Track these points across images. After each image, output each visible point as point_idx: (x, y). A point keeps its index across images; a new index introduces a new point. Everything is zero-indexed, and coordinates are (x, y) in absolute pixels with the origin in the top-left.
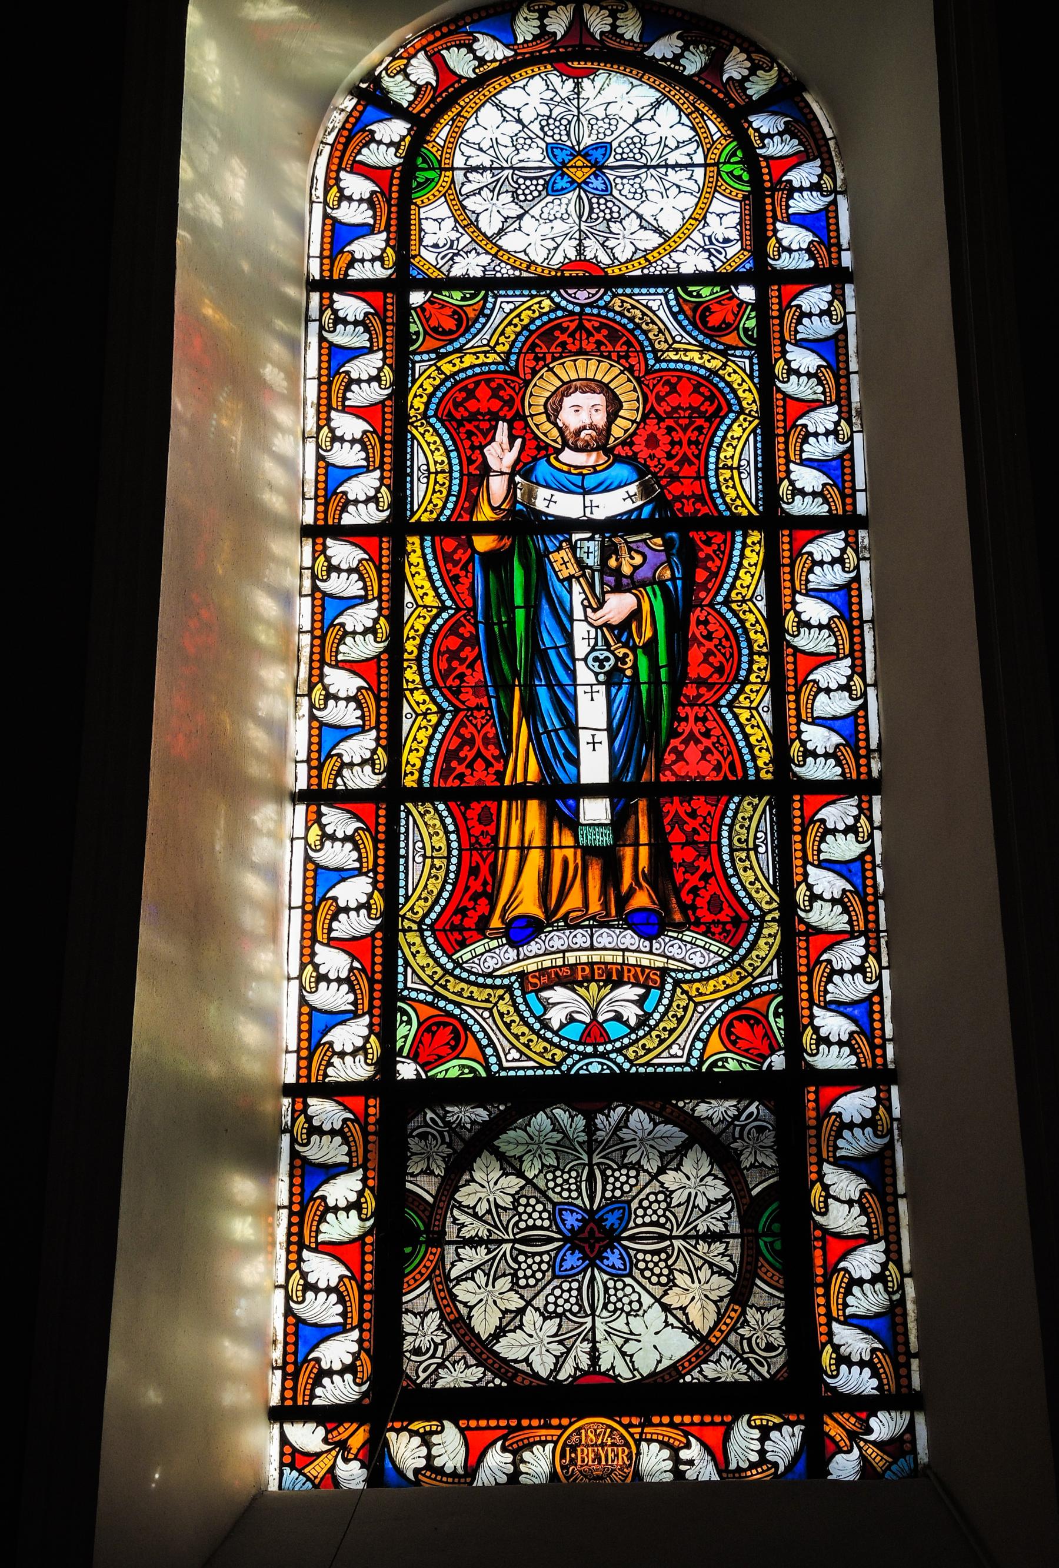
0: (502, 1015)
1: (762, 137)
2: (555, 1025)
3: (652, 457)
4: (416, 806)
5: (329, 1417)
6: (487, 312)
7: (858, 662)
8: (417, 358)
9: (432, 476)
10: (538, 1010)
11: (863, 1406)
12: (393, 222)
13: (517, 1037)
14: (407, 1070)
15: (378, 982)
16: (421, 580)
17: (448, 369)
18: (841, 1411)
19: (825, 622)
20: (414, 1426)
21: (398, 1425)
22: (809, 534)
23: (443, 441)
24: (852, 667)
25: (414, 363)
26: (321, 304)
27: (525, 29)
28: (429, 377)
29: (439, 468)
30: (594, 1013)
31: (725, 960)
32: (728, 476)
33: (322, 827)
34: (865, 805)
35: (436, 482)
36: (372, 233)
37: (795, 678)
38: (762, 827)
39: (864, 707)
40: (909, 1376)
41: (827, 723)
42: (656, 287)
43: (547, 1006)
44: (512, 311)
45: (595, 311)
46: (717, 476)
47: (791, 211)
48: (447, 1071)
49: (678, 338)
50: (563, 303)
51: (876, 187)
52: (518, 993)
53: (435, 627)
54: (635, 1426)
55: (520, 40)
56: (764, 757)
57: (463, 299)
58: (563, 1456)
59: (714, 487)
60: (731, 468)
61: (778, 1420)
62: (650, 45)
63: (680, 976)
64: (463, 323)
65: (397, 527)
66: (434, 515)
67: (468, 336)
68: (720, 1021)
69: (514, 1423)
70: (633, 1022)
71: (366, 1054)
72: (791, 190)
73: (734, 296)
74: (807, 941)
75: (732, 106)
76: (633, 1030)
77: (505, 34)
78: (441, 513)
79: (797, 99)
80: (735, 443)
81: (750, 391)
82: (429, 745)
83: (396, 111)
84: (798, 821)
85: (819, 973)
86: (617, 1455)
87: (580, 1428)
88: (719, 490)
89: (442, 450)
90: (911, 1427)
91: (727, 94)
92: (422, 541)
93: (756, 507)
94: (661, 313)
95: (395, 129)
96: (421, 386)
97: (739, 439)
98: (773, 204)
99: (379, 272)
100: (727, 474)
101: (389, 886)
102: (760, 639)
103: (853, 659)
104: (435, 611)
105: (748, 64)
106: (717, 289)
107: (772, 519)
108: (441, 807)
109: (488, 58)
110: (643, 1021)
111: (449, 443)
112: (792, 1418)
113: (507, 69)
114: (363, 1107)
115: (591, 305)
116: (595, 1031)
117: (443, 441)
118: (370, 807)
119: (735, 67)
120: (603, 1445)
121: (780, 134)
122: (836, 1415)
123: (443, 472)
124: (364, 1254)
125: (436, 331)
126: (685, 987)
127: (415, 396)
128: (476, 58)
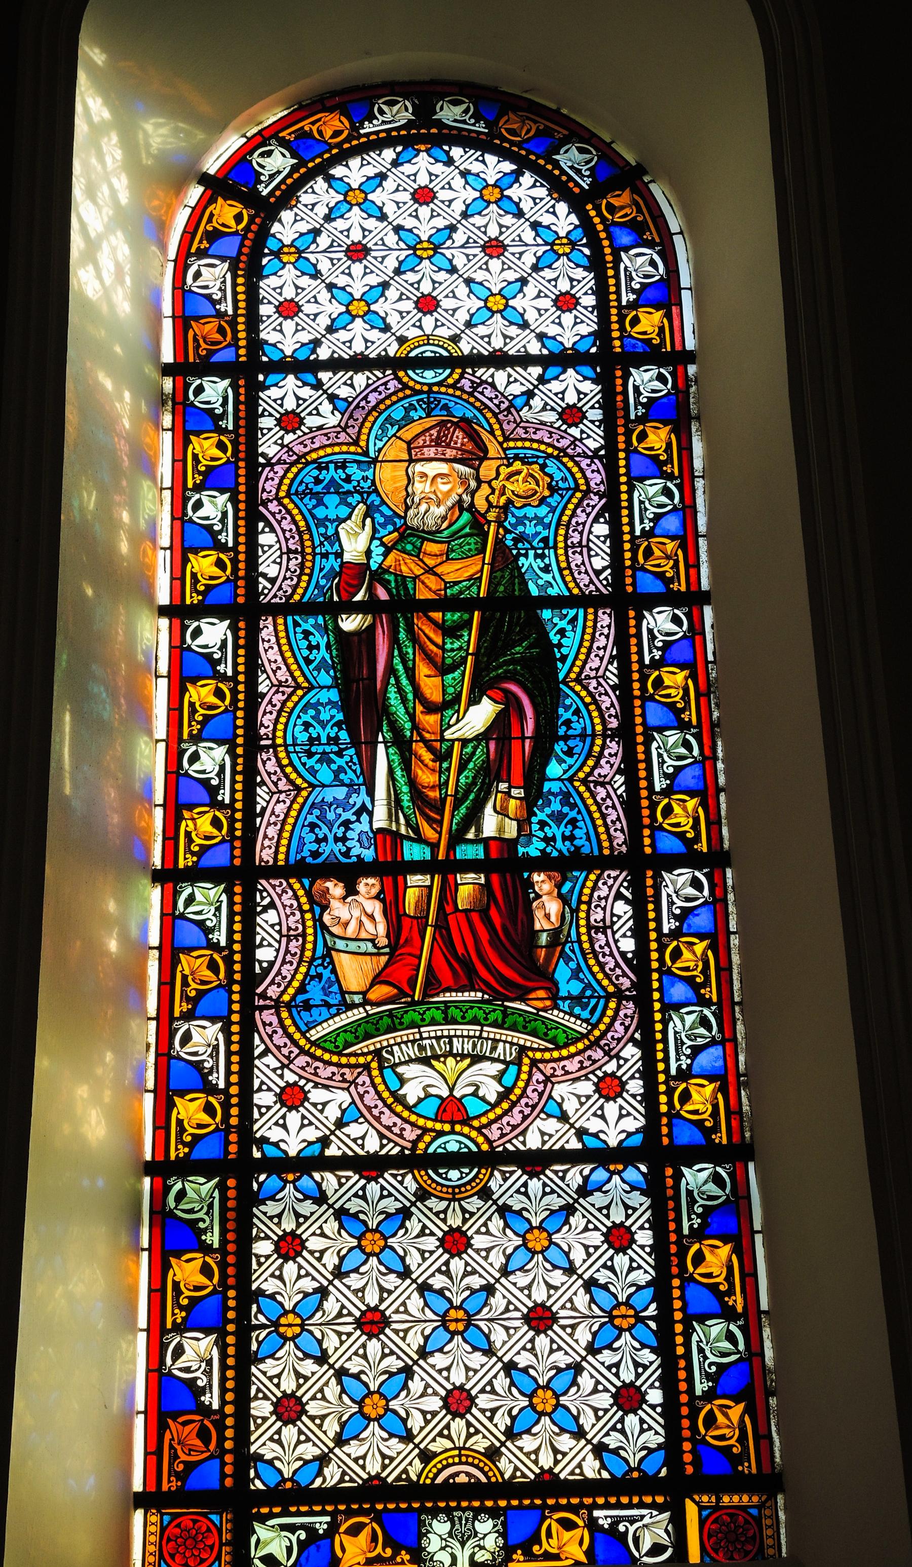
2: (411, 1100)
10: (394, 1084)
15: (230, 1368)
16: (273, 654)
30: (451, 1090)
43: (402, 1081)
45: (443, 389)
50: (474, 1134)
51: (721, 267)
52: (375, 1073)
56: (620, 838)
63: (538, 1055)
70: (492, 1098)
76: (493, 1106)
81: (264, 1024)
110: (503, 1096)
114: (217, 1475)
115: (441, 1134)
116: (451, 1108)
124: (231, 1002)
126: (541, 1066)
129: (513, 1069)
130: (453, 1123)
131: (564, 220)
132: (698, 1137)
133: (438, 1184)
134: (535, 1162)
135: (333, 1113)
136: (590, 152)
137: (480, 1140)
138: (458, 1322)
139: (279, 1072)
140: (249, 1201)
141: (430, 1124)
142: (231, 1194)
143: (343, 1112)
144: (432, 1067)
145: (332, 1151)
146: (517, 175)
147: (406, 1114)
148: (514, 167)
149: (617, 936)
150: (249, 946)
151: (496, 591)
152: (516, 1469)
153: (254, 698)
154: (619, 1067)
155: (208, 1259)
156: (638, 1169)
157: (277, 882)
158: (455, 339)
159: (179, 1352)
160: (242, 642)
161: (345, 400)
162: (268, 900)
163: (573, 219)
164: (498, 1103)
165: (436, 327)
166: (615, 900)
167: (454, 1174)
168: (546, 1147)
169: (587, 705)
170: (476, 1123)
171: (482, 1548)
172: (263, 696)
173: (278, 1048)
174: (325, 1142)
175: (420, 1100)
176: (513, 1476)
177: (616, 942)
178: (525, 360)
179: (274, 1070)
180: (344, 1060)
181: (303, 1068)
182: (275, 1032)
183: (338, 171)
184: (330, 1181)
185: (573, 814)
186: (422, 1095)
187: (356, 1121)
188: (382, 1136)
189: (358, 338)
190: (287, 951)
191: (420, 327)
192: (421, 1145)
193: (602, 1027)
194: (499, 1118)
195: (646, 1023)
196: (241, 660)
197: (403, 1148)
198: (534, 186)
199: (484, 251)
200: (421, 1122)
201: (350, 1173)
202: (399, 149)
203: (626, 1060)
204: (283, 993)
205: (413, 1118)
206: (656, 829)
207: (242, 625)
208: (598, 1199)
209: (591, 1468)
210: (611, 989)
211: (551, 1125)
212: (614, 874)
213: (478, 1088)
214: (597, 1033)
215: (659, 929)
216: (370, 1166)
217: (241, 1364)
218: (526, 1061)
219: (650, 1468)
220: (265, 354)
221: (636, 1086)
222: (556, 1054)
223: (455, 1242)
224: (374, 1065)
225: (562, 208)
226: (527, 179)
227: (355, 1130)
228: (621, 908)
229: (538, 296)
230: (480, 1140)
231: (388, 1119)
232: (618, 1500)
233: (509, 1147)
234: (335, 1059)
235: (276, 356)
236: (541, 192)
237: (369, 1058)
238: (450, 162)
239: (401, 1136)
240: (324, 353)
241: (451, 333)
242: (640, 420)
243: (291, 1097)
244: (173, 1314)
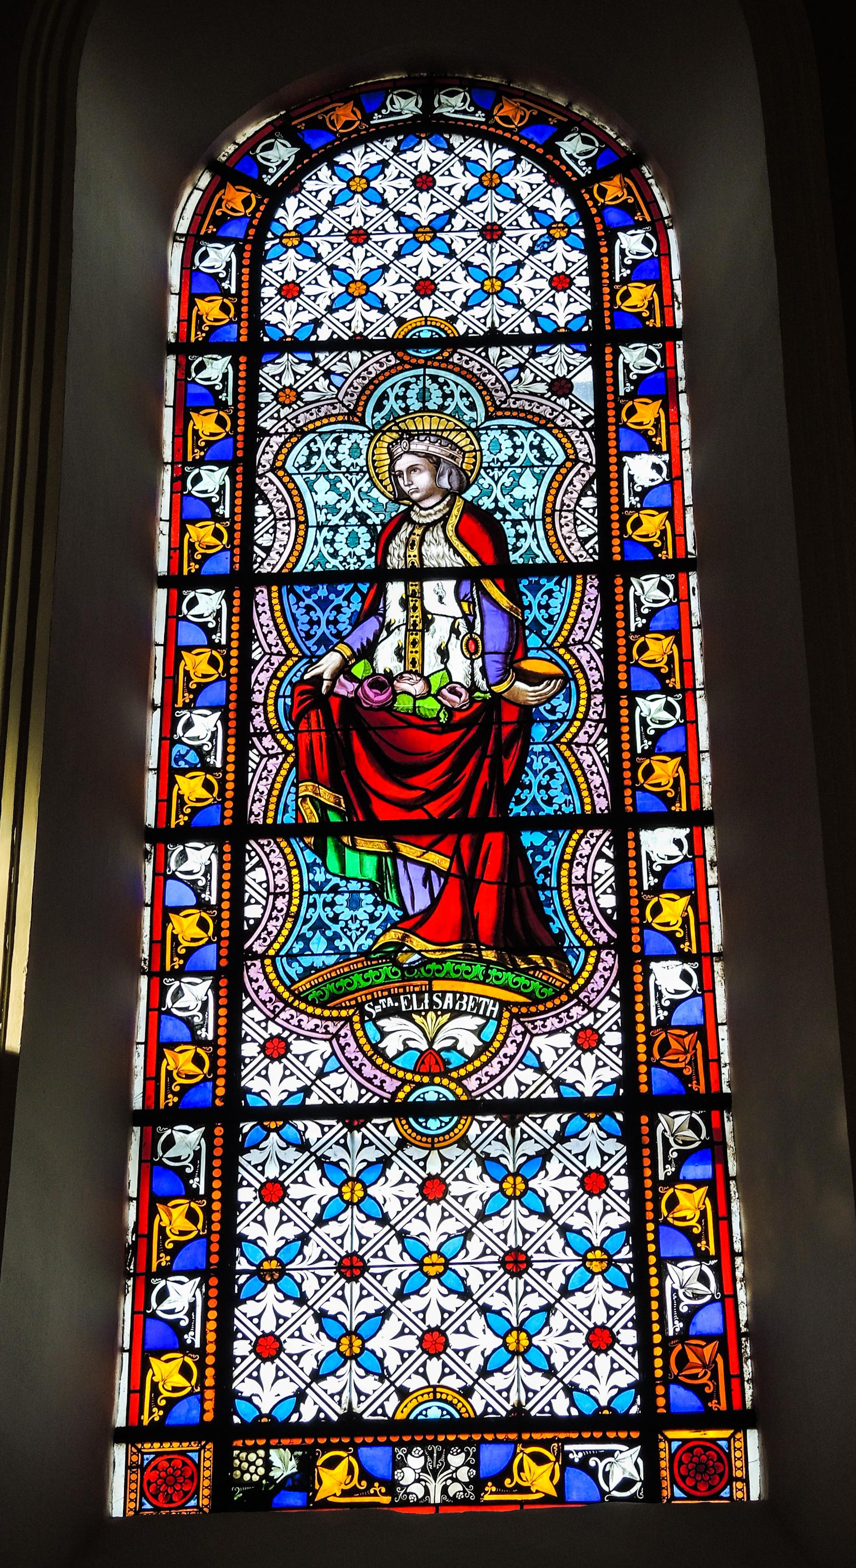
2: (391, 1053)
3: (354, 919)
30: (431, 1043)
50: (453, 1086)
52: (357, 1026)
70: (470, 1052)
76: (471, 1060)
102: (594, 676)
110: (479, 1052)
115: (420, 1085)
123: (578, 887)
129: (493, 1024)
130: (432, 1076)
131: (559, 205)
132: (674, 1082)
133: (418, 1133)
134: (512, 1112)
135: (315, 1063)
136: (593, 144)
137: (459, 1091)
138: (434, 1265)
139: (263, 1024)
140: (235, 1148)
141: (409, 1076)
142: (218, 1142)
143: (325, 1061)
144: (413, 1021)
145: (313, 1100)
146: (517, 160)
147: (386, 1066)
148: (512, 154)
149: (597, 893)
150: (238, 902)
152: (488, 1405)
153: (247, 665)
154: (596, 1020)
155: (193, 1205)
156: (614, 1117)
157: (265, 842)
158: (452, 320)
159: (164, 1295)
160: (236, 610)
161: (341, 375)
162: (257, 859)
163: (569, 204)
164: (477, 1056)
165: (434, 309)
166: (597, 858)
167: (433, 1124)
168: (524, 1096)
169: (282, 680)
171: (456, 1480)
172: (256, 663)
173: (264, 1003)
174: (306, 1091)
175: (399, 1054)
176: (485, 1412)
177: (596, 898)
178: (520, 339)
179: (259, 1023)
180: (327, 1013)
181: (287, 1021)
182: (261, 987)
183: (343, 159)
184: (313, 1131)
186: (401, 1049)
187: (336, 1071)
188: (360, 1086)
189: (358, 317)
190: (274, 908)
191: (418, 309)
192: (401, 1095)
194: (595, 969)
195: (625, 977)
196: (235, 627)
197: (382, 1098)
198: (531, 172)
199: (481, 235)
200: (401, 1074)
201: (333, 1122)
202: (400, 137)
203: (603, 1013)
204: (270, 946)
205: (393, 1071)
206: (636, 788)
207: (237, 594)
208: (575, 1146)
209: (561, 1406)
210: (590, 943)
211: (528, 1076)
212: (597, 833)
213: (457, 1041)
215: (640, 886)
216: (353, 1116)
217: (225, 1299)
219: (621, 1405)
220: (266, 335)
221: (614, 1038)
223: (433, 1189)
224: (356, 1018)
225: (559, 193)
226: (525, 165)
227: (335, 1080)
228: (602, 866)
229: (534, 277)
230: (459, 1091)
231: (368, 1071)
232: (655, 1299)
233: (487, 1097)
234: (318, 1011)
235: (276, 336)
236: (538, 178)
237: (351, 1011)
238: (450, 149)
239: (381, 1088)
240: (324, 334)
241: (448, 314)
242: (629, 396)
243: (276, 1049)
244: (159, 1258)
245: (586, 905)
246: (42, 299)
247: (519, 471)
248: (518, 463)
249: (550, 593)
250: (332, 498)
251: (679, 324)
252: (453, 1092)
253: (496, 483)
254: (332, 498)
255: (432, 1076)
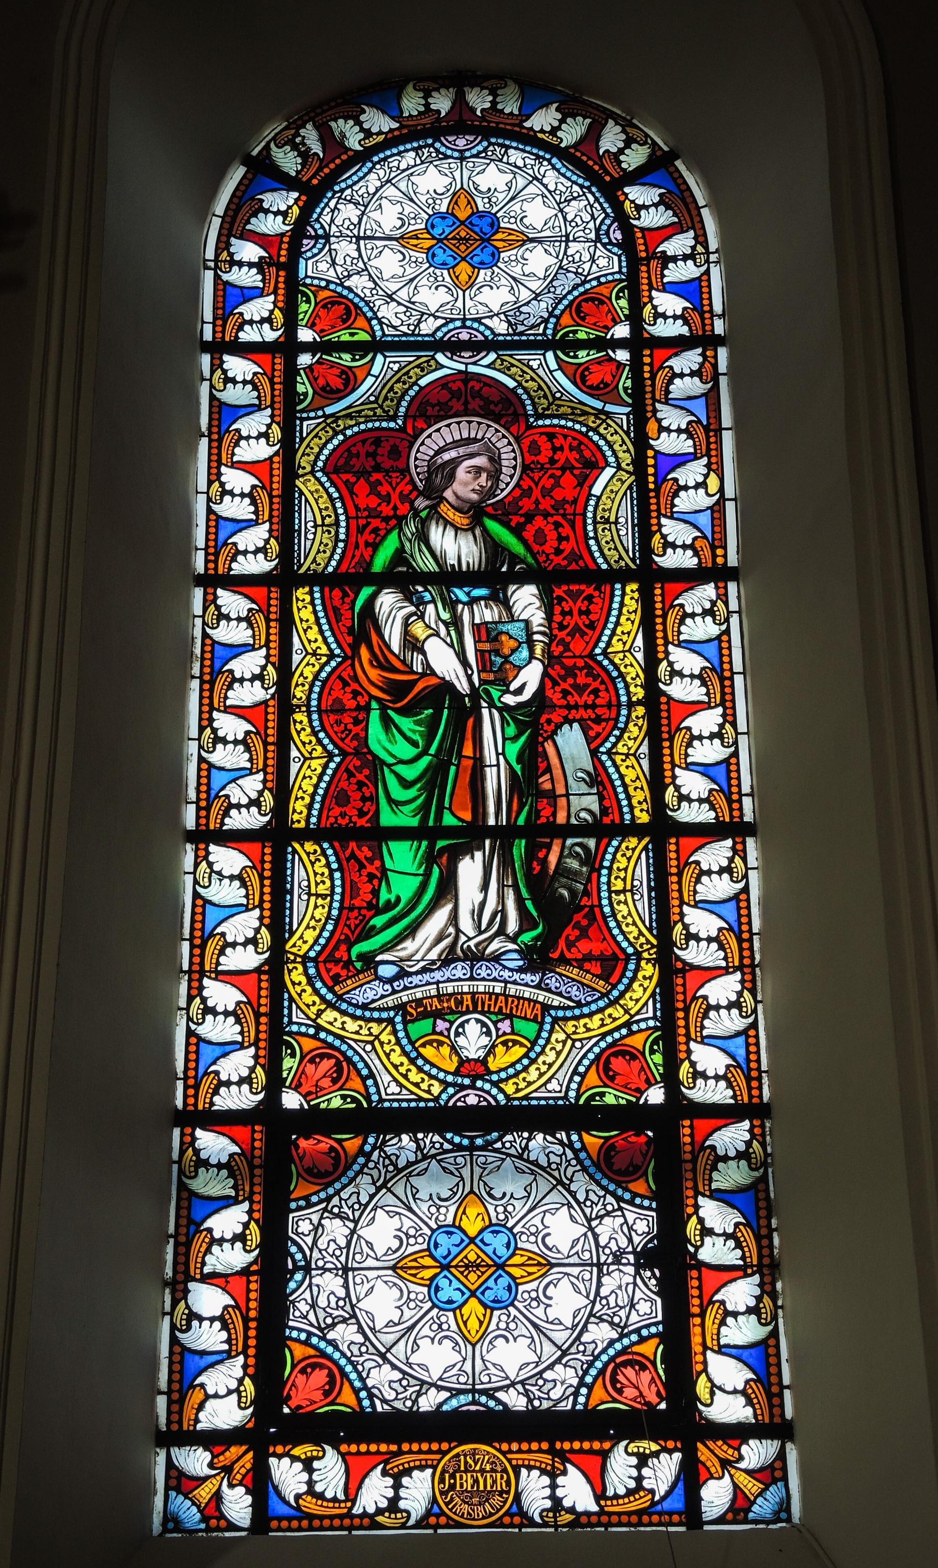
0: (545, 397)
1: (639, 208)
4: (302, 846)
5: (214, 1440)
6: (577, 1078)
7: (729, 711)
8: (651, 1023)
9: (628, 887)
11: (738, 1433)
12: (281, 285)
13: (532, 379)
14: (291, 1100)
17: (617, 1012)
18: (715, 1439)
19: (697, 672)
20: (296, 1452)
21: (280, 1449)
22: (679, 586)
23: (619, 926)
24: (724, 715)
25: (654, 1017)
26: (212, 365)
27: (411, 104)
28: (637, 1001)
29: (622, 897)
31: (603, 996)
32: (321, 886)
33: (210, 865)
34: (739, 847)
35: (624, 880)
36: (261, 296)
37: (669, 725)
38: (309, 543)
39: (736, 754)
40: (782, 1405)
41: (705, 770)
42: (390, 1108)
44: (549, 1081)
46: (333, 886)
47: (665, 280)
48: (329, 1100)
49: (368, 1048)
52: (399, 1027)
53: (324, 675)
54: (496, 1141)
55: (406, 114)
57: (602, 1095)
58: (442, 1481)
59: (337, 875)
60: (318, 895)
61: (654, 1447)
62: (528, 117)
63: (560, 1014)
64: (350, 380)
65: (286, 577)
66: (624, 846)
67: (597, 1050)
68: (598, 1057)
69: (394, 1448)
71: (251, 1084)
72: (666, 260)
73: (305, 1097)
74: (684, 978)
75: (608, 178)
77: (391, 108)
78: (617, 849)
79: (672, 169)
80: (313, 923)
81: (294, 983)
82: (618, 617)
83: (287, 182)
84: (674, 863)
85: (694, 1009)
86: (495, 1482)
87: (458, 1455)
88: (331, 872)
89: (619, 917)
90: (781, 1456)
91: (602, 167)
92: (311, 593)
93: (295, 851)
94: (387, 1078)
95: (282, 200)
96: (645, 990)
97: (308, 927)
98: (648, 272)
99: (270, 335)
100: (322, 889)
101: (278, 924)
103: (725, 708)
104: (324, 659)
105: (624, 137)
106: (323, 1106)
107: (648, 575)
108: (604, 566)
109: (375, 130)
111: (612, 924)
112: (670, 1444)
113: (392, 141)
115: (463, 1087)
117: (619, 926)
118: (256, 847)
119: (611, 139)
120: (482, 1471)
121: (656, 205)
122: (710, 1444)
123: (618, 893)
124: (260, 988)
125: (632, 1055)
127: (651, 978)
128: (362, 130)
141: (450, 1078)
151: (538, 816)
170: (495, 1078)
185: (596, 684)
193: (621, 987)
214: (615, 993)
218: (548, 1019)
222: (577, 1012)
245: (612, 545)
246: (34, 860)
247: (558, 473)
248: (558, 465)
249: (590, 598)
250: (373, 502)
251: (748, 817)
252: (494, 1098)
253: (537, 484)
254: (373, 502)
255: (474, 1079)
